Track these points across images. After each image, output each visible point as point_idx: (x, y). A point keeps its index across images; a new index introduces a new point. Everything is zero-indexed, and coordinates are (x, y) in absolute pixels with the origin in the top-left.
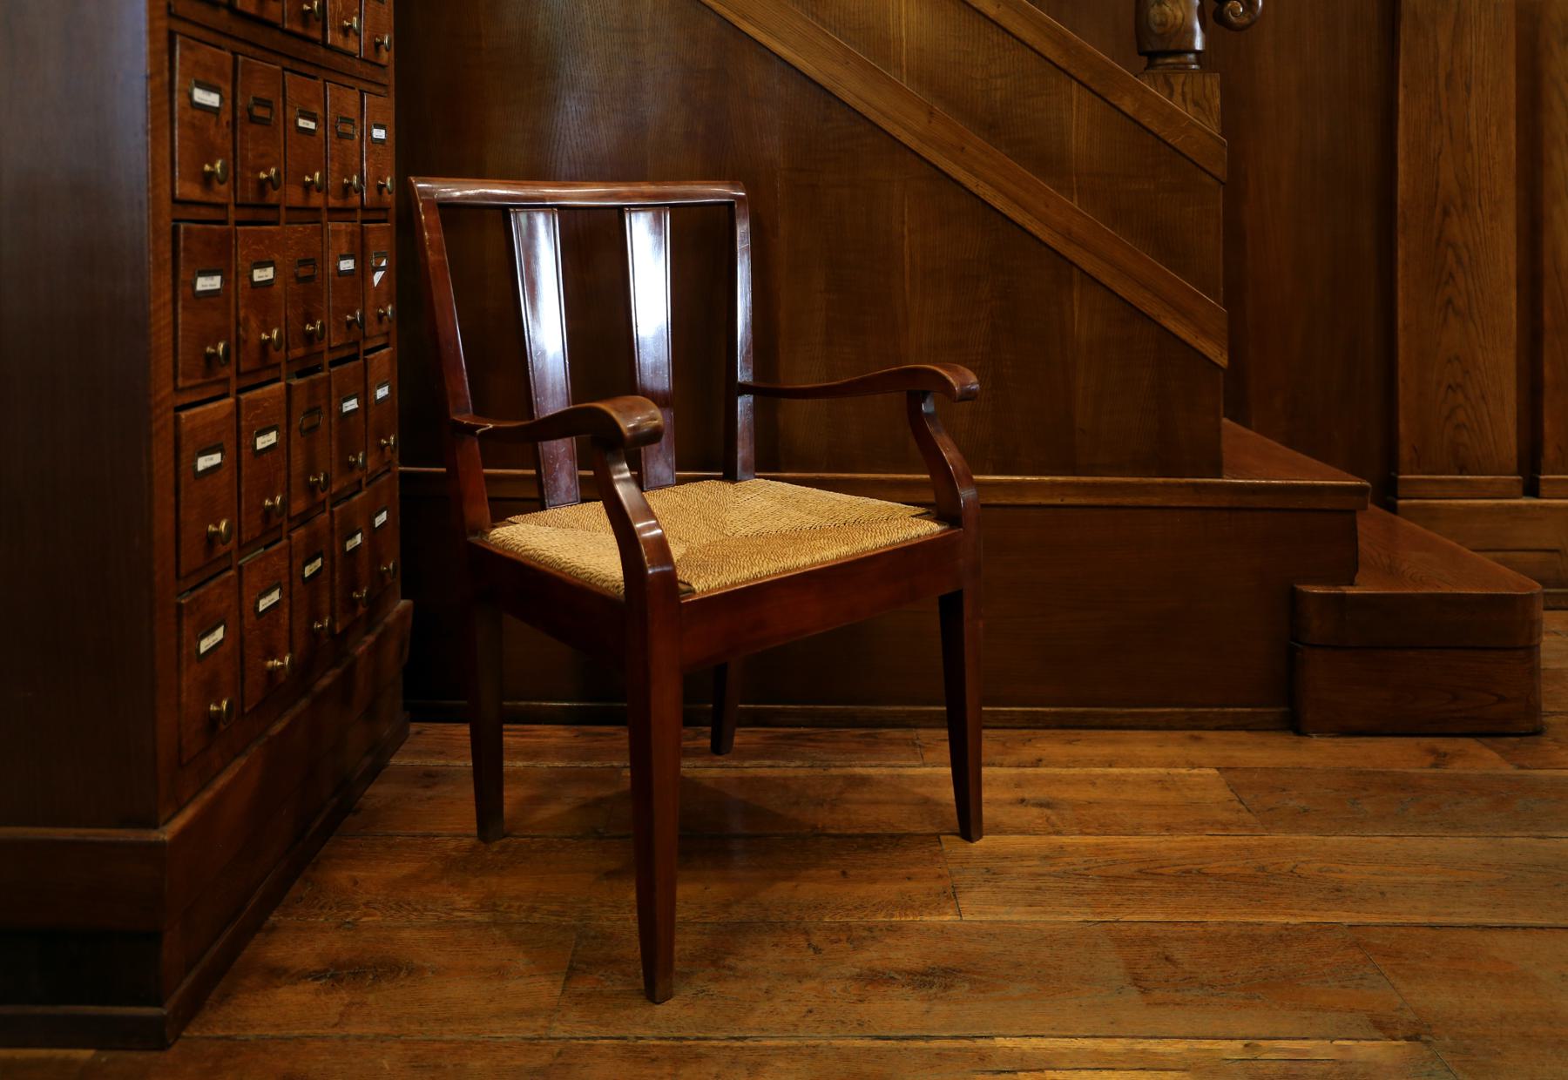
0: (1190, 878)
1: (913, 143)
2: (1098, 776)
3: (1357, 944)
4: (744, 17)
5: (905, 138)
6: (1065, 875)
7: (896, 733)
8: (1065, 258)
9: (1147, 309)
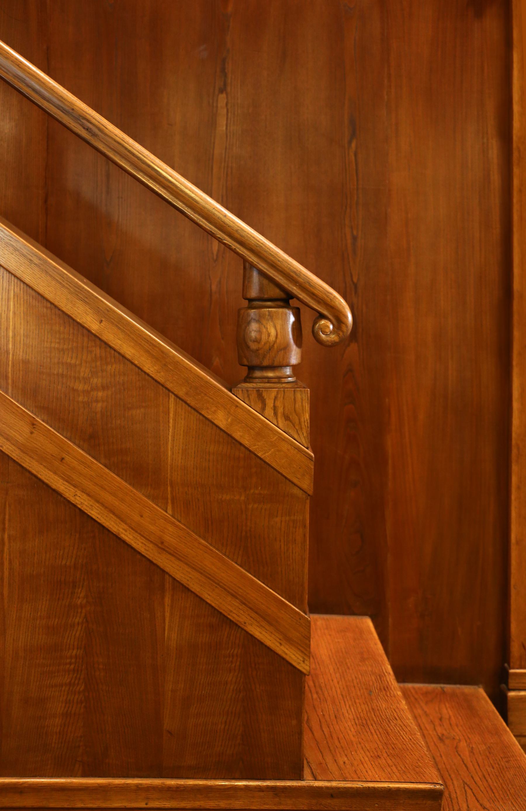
9: (233, 617)
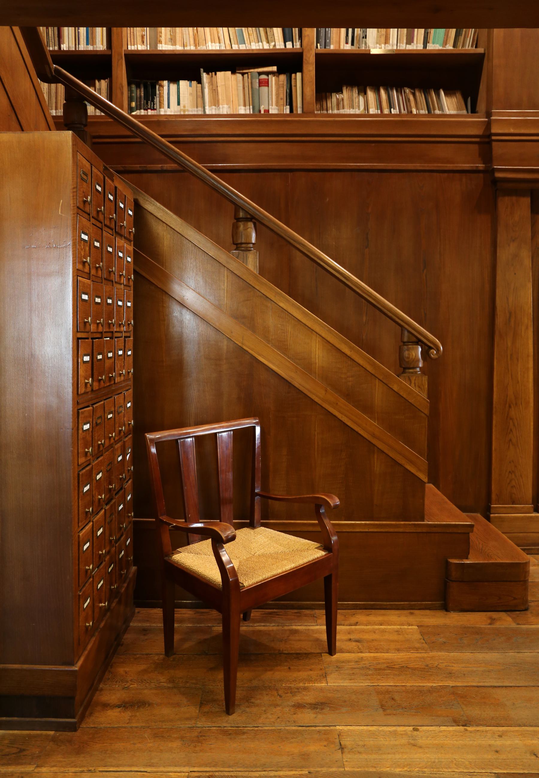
0: (403, 669)
1: (319, 402)
2: (376, 629)
3: (453, 693)
4: (259, 355)
5: (317, 400)
6: (362, 668)
7: (307, 612)
8: (372, 443)
9: (400, 462)
